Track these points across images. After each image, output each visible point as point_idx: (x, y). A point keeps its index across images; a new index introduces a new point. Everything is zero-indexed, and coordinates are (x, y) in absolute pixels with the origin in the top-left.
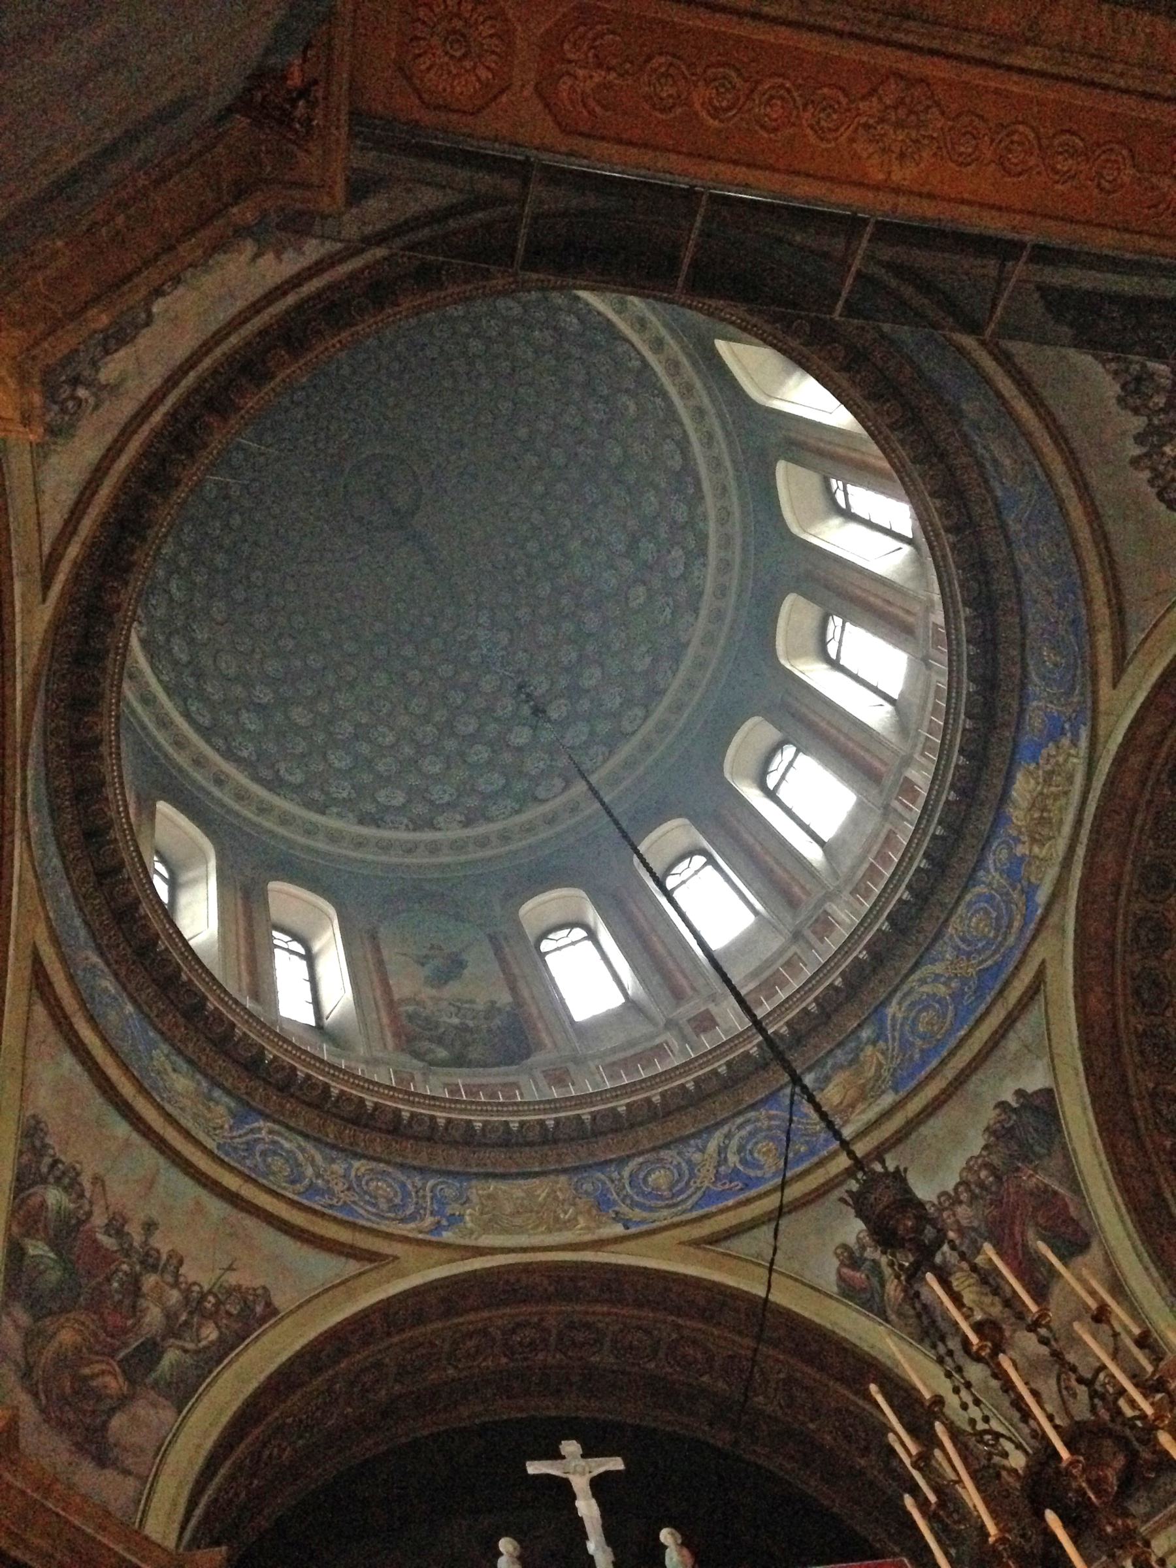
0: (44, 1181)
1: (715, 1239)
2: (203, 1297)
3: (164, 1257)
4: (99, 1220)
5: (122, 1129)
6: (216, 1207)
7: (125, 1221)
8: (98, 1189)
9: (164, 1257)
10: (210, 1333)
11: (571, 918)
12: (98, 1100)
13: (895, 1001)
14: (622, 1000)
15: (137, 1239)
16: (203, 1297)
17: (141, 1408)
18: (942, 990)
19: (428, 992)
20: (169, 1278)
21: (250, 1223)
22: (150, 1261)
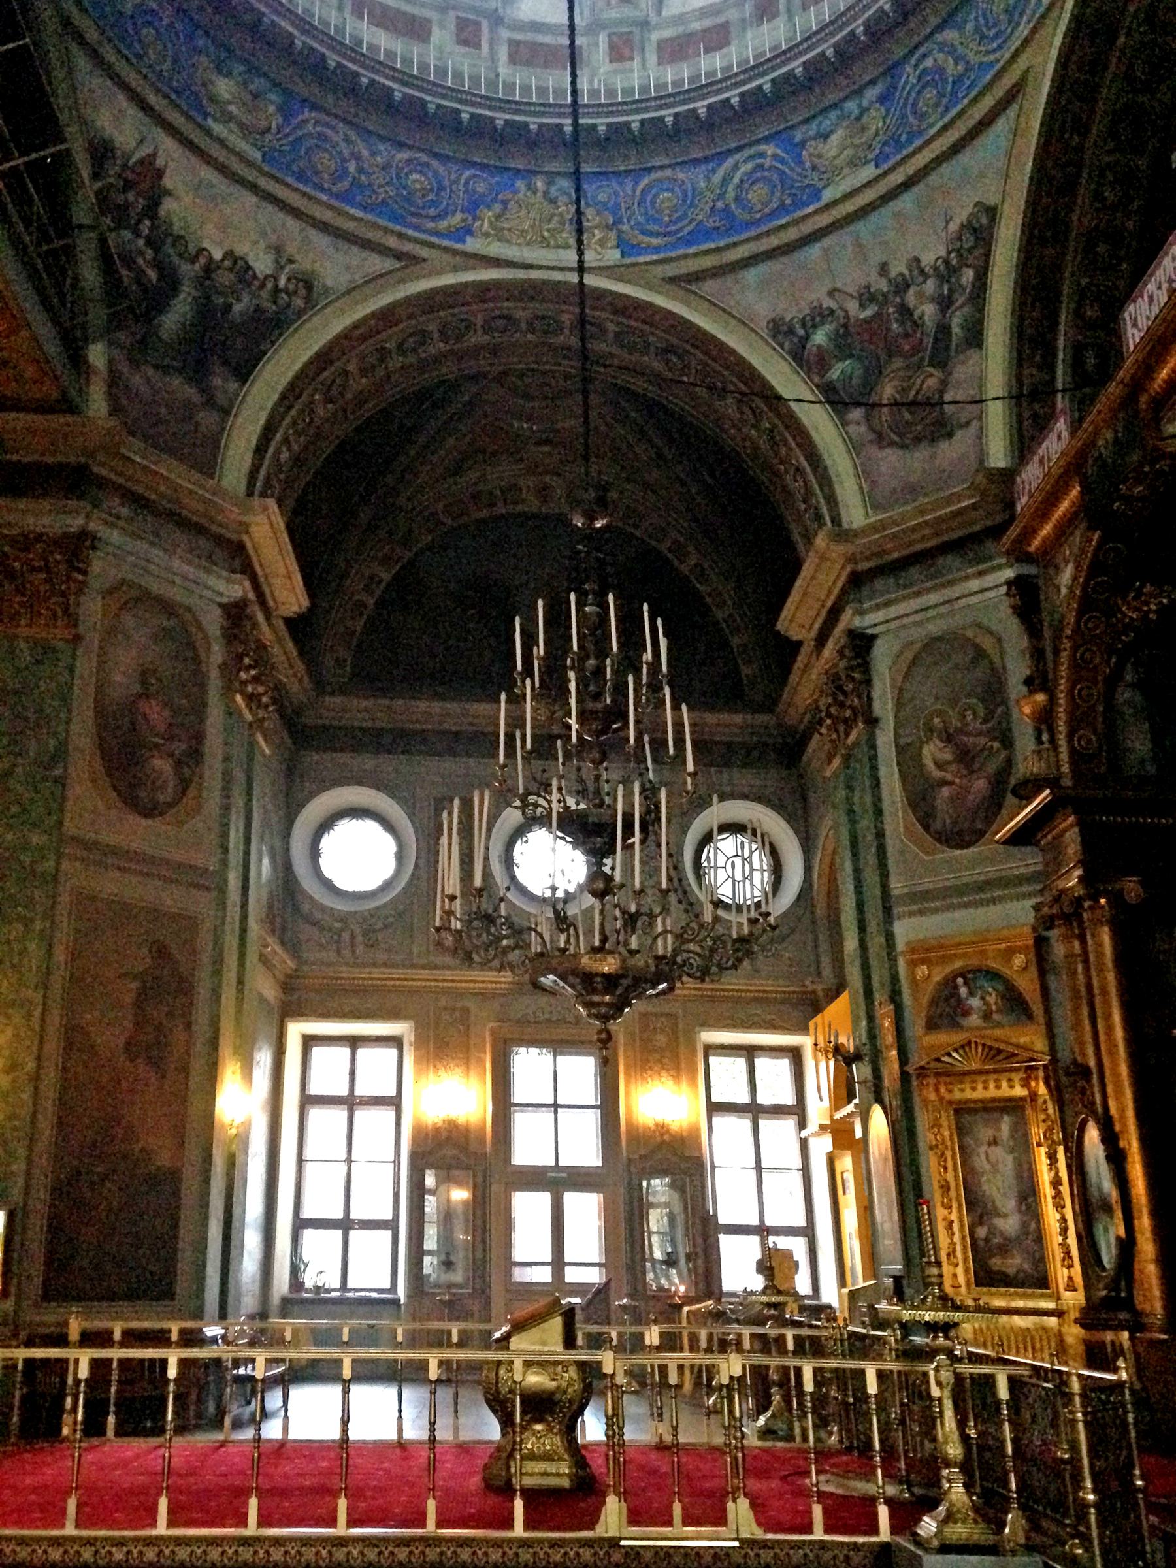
0: (807, 337)
3: (907, 273)
4: (853, 306)
5: (814, 251)
6: (906, 202)
7: (868, 287)
9: (907, 273)
10: (968, 275)
14: (336, 1435)
16: (947, 262)
18: (352, 167)
20: (921, 279)
21: (933, 179)
22: (902, 286)
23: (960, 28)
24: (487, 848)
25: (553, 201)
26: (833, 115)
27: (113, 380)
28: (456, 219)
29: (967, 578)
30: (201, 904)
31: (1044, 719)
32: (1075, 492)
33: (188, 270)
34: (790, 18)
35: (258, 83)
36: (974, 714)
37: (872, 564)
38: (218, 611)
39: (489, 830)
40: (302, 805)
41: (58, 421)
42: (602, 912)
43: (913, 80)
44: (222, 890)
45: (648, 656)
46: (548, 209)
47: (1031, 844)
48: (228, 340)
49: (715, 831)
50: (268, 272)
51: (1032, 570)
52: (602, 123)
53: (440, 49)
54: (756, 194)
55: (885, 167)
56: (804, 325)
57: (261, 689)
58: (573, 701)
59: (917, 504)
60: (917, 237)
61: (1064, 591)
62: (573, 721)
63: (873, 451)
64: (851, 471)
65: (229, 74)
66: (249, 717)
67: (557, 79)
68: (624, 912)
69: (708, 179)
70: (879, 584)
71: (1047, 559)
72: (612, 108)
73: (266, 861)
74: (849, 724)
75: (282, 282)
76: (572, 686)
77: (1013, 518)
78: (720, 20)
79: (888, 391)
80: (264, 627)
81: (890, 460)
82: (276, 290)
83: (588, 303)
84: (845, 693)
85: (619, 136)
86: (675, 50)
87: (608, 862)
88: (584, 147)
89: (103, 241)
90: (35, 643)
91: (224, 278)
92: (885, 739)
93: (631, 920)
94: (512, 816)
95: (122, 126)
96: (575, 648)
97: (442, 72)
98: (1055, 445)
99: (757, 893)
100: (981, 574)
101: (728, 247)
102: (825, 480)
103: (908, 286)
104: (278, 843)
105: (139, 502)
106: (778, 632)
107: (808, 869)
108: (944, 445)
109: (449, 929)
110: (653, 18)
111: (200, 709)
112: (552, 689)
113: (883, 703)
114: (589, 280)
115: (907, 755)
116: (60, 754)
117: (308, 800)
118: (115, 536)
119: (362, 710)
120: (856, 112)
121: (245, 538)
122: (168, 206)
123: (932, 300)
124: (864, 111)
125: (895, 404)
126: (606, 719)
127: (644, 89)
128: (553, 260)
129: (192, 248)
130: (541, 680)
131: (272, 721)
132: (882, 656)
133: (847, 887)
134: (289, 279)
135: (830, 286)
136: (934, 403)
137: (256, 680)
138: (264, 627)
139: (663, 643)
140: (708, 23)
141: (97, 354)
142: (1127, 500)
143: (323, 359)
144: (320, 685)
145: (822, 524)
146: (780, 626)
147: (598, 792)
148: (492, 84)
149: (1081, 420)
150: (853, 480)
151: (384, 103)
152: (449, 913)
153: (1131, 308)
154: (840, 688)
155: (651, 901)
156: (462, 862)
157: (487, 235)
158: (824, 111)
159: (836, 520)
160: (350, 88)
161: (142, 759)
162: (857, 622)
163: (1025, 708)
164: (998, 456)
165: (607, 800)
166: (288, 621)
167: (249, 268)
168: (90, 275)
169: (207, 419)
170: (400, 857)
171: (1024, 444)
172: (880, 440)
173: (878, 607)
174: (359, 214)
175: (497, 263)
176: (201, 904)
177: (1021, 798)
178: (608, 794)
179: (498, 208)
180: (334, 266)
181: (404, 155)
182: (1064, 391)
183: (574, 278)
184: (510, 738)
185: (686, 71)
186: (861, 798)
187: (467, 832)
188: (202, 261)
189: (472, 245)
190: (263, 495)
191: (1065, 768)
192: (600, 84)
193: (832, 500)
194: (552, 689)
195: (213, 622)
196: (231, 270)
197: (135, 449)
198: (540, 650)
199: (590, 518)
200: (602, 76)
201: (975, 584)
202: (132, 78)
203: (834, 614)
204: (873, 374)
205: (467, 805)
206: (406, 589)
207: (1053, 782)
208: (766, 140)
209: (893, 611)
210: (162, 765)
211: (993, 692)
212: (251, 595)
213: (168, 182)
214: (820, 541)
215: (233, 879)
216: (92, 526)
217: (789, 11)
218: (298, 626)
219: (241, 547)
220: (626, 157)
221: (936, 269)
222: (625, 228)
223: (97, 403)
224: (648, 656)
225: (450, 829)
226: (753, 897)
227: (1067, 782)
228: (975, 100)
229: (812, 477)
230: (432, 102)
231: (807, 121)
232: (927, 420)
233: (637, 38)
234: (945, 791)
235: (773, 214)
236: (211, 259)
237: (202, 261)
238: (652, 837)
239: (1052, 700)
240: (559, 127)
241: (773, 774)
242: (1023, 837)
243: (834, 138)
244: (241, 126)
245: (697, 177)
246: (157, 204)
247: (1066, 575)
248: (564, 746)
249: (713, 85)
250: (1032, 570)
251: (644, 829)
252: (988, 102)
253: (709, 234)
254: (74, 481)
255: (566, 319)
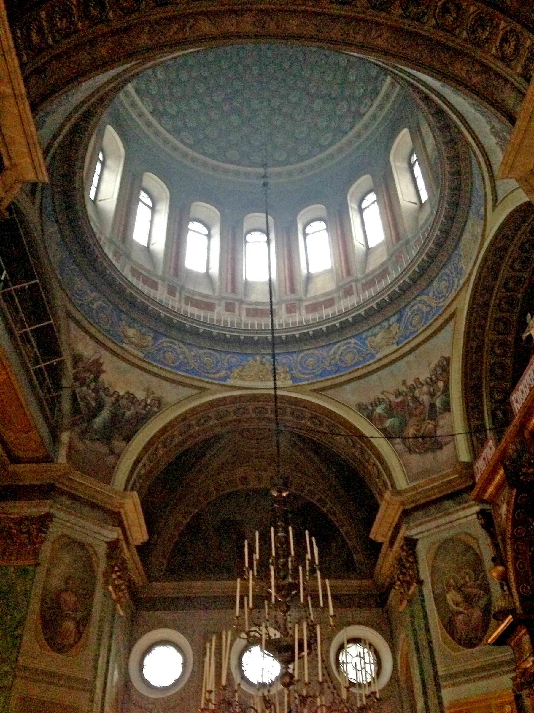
1: (495, 200)
2: (431, 379)
3: (414, 384)
4: (392, 398)
5: (374, 377)
7: (398, 390)
8: (385, 393)
9: (414, 384)
10: (441, 384)
11: (155, 194)
12: (362, 381)
13: (167, 339)
15: (405, 389)
16: (431, 379)
17: (442, 422)
18: (181, 357)
19: (441, 88)
20: (420, 386)
21: (421, 348)
22: (412, 389)
23: (428, 295)
24: (229, 658)
25: (264, 365)
26: (378, 328)
27: (71, 447)
28: (223, 373)
29: (457, 511)
30: (80, 700)
31: (504, 578)
32: (502, 472)
33: (108, 401)
34: (358, 295)
35: (144, 330)
36: (470, 578)
37: (413, 505)
38: (105, 545)
39: (231, 649)
40: (136, 640)
41: (43, 466)
42: (289, 695)
43: (409, 314)
44: (92, 692)
45: (309, 556)
46: (261, 367)
47: (506, 645)
48: (122, 427)
49: (346, 642)
50: (143, 398)
51: (488, 507)
52: (283, 335)
53: (219, 314)
54: (348, 357)
55: (401, 345)
56: (371, 405)
57: (121, 582)
58: (273, 581)
59: (430, 478)
60: (418, 369)
61: (504, 516)
62: (273, 591)
63: (408, 456)
64: (398, 465)
65: (134, 327)
66: (114, 596)
67: (265, 321)
68: (300, 696)
69: (328, 352)
70: (416, 514)
71: (492, 501)
72: (287, 329)
73: (116, 673)
74: (409, 584)
75: (148, 402)
76: (272, 573)
77: (474, 484)
78: (331, 297)
79: (411, 431)
80: (126, 550)
81: (415, 459)
82: (146, 405)
83: (278, 401)
84: (405, 568)
85: (291, 340)
86: (314, 308)
87: (291, 666)
88: (276, 344)
89: (74, 392)
90: (17, 568)
91: (123, 402)
92: (427, 590)
93: (303, 700)
94: (241, 642)
95: (87, 349)
96: (274, 554)
97: (219, 321)
98: (489, 451)
99: (369, 677)
100: (464, 509)
101: (337, 377)
102: (386, 468)
103: (415, 388)
104: (123, 663)
105: (74, 498)
106: (371, 539)
107: (394, 659)
108: (438, 453)
109: (208, 710)
110: (304, 298)
111: (91, 594)
112: (263, 575)
113: (425, 573)
114: (279, 392)
115: (440, 600)
116: (20, 623)
117: (139, 638)
118: (61, 515)
119: (169, 588)
120: (387, 326)
121: (122, 511)
122: (103, 377)
123: (427, 394)
124: (390, 326)
125: (416, 437)
126: (288, 590)
127: (301, 322)
128: (264, 386)
129: (111, 392)
130: (258, 571)
131: (126, 597)
132: (421, 548)
133: (416, 672)
134: (152, 400)
135: (381, 390)
136: (432, 435)
137: (119, 577)
138: (126, 550)
139: (316, 549)
140: (324, 299)
141: (65, 437)
142: (526, 474)
143: (164, 430)
144: (150, 579)
145: (387, 488)
146: (372, 536)
147: (286, 629)
148: (239, 324)
149: (500, 440)
150: (400, 470)
151: (195, 333)
152: (209, 701)
153: (514, 395)
154: (403, 566)
155: (315, 689)
156: (216, 667)
157: (236, 378)
158: (375, 326)
159: (393, 486)
160: (181, 328)
161: (61, 625)
162: (408, 533)
163: (494, 573)
164: (465, 457)
165: (290, 632)
166: (137, 547)
167: (135, 397)
168: (66, 406)
169: (110, 459)
170: (184, 665)
171: (476, 451)
172: (410, 451)
173: (417, 526)
174: (183, 373)
175: (240, 388)
176: (80, 700)
177: (498, 620)
178: (290, 628)
179: (240, 368)
180: (171, 393)
181: (202, 351)
182: (490, 429)
183: (272, 392)
184: (242, 598)
185: (317, 315)
186: (419, 622)
187: (219, 648)
188: (115, 396)
189: (230, 382)
190: (132, 489)
191: (518, 604)
192: (282, 321)
193: (390, 476)
194: (263, 575)
195: (102, 550)
196: (127, 399)
197: (77, 477)
198: (256, 556)
199: (280, 491)
200: (283, 318)
201: (462, 514)
202: (93, 330)
203: (397, 528)
204: (404, 424)
205: (220, 638)
206: (194, 529)
207: (512, 611)
208: (350, 338)
209: (424, 527)
210: (70, 625)
211: (477, 564)
212: (121, 537)
213: (104, 368)
214: (387, 495)
215: (99, 683)
216: (52, 511)
217: (357, 292)
218: (143, 550)
219: (119, 514)
220: (294, 346)
221: (427, 382)
222: (294, 372)
223: (62, 458)
224: (309, 556)
225: (210, 652)
226: (366, 678)
227: (520, 611)
228: (435, 321)
229: (380, 467)
230: (215, 332)
231: (368, 330)
232: (430, 442)
233: (297, 305)
234: (460, 617)
235: (355, 364)
236: (119, 396)
237: (115, 396)
238: (314, 652)
239: (506, 568)
240: (267, 338)
241: (374, 611)
242: (501, 641)
243: (379, 336)
244: (136, 345)
245: (323, 352)
246: (98, 377)
247: (504, 509)
248: (268, 605)
249: (328, 320)
250: (488, 507)
251: (309, 647)
252: (441, 321)
253: (330, 373)
254: (47, 491)
255: (269, 408)
